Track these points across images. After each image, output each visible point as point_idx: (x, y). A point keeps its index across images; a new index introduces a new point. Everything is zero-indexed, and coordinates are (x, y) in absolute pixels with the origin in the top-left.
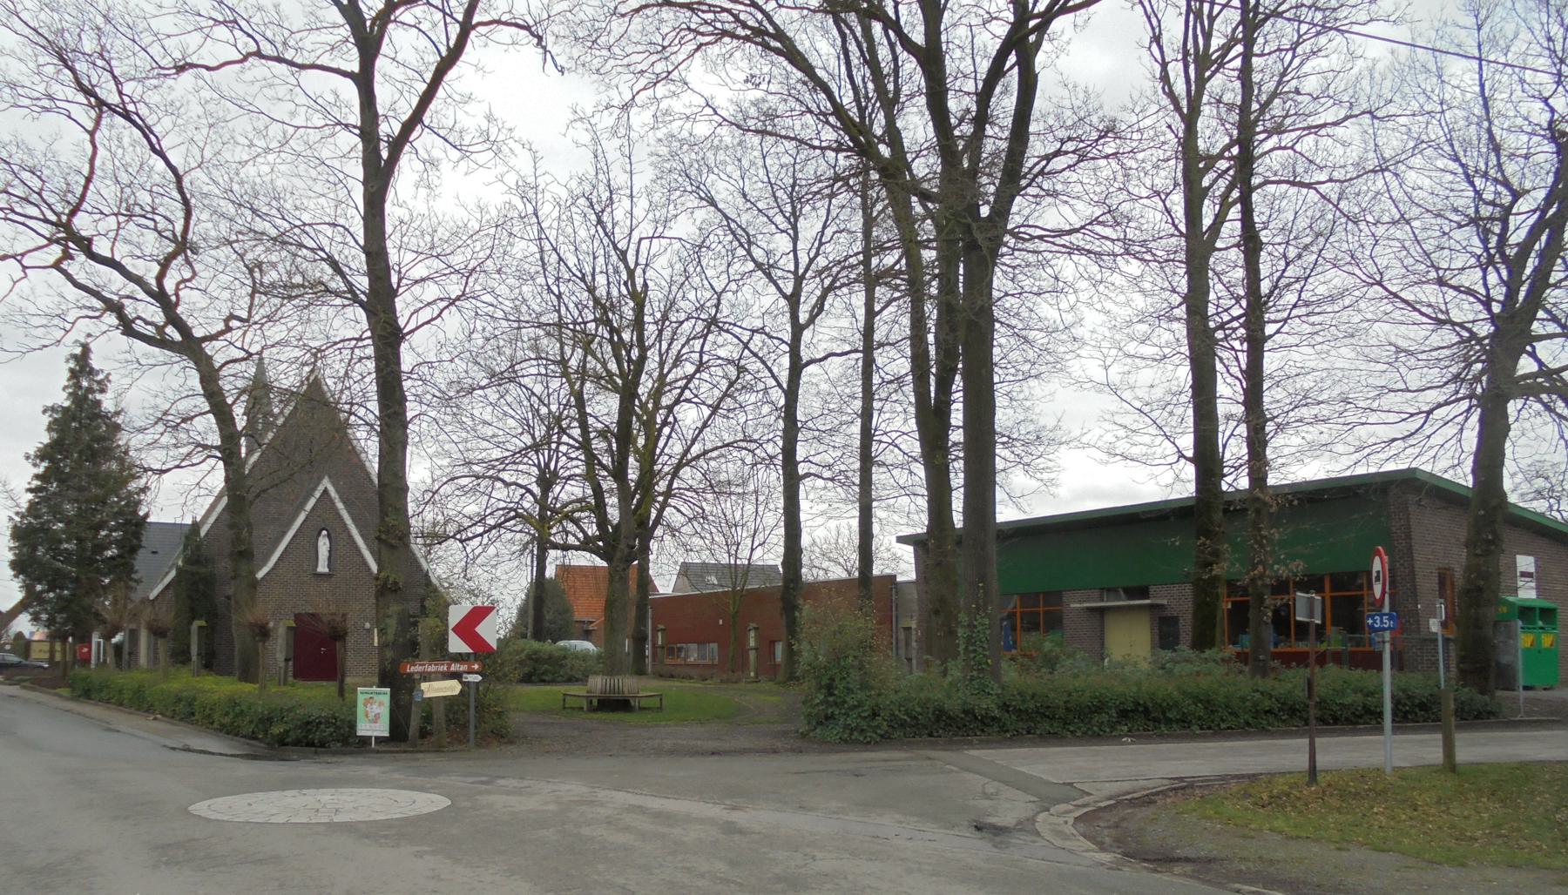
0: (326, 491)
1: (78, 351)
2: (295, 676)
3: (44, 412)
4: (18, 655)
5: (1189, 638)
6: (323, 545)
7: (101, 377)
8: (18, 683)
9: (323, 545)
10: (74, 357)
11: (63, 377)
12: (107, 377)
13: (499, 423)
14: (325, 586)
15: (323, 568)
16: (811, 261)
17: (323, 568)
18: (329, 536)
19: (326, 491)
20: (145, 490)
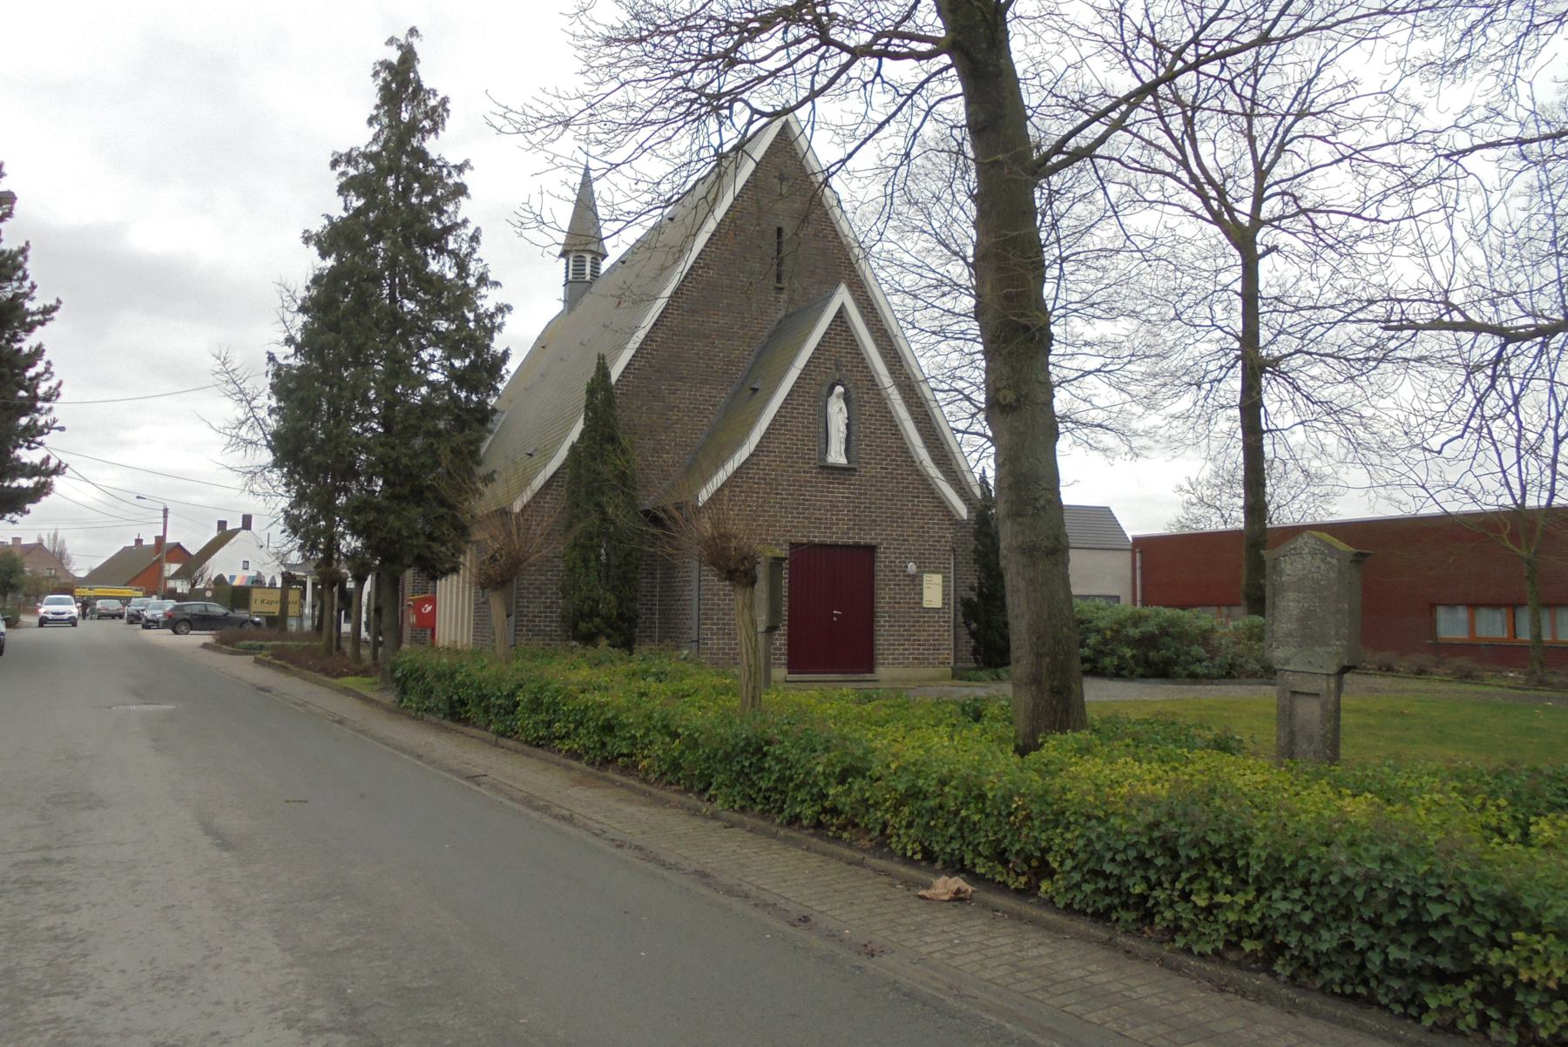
0: (841, 312)
1: (394, 56)
2: (793, 667)
3: (334, 164)
4: (224, 605)
5: (784, 659)
6: (837, 414)
7: (432, 102)
8: (248, 651)
9: (837, 414)
10: (386, 65)
11: (369, 96)
12: (444, 101)
13: (1073, 222)
14: (839, 492)
15: (837, 456)
16: (1168, 131)
17: (837, 456)
18: (847, 398)
19: (841, 312)
20: (503, 309)
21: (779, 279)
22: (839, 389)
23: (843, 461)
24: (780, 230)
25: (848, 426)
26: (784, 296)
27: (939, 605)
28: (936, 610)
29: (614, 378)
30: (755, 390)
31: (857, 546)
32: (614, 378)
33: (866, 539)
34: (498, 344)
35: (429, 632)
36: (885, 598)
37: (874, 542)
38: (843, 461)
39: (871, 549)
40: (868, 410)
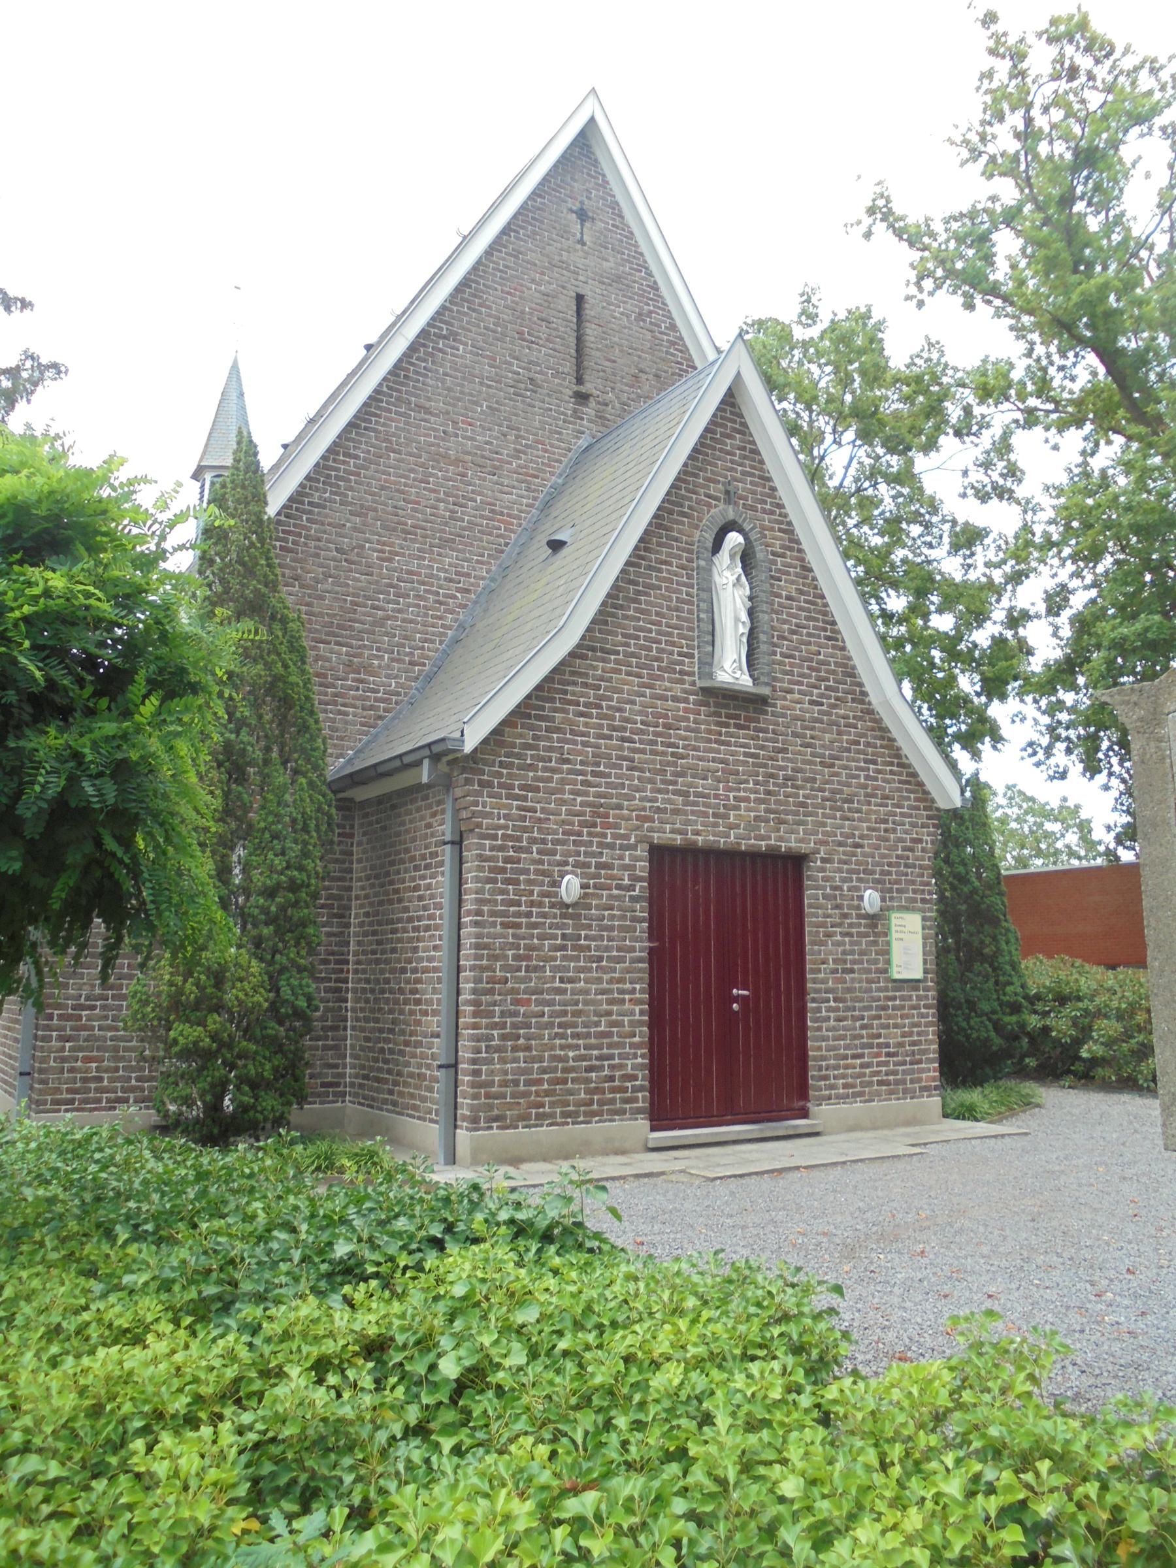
5: (642, 1099)
15: (731, 669)
18: (747, 558)
21: (580, 380)
22: (734, 539)
23: (745, 681)
24: (580, 299)
25: (751, 613)
26: (589, 411)
27: (919, 975)
28: (914, 984)
29: (272, 510)
30: (556, 546)
31: (1144, 947)
32: (272, 510)
33: (791, 843)
34: (813, 1108)
35: (361, 794)
36: (823, 957)
37: (804, 848)
38: (745, 681)
39: (796, 863)
40: (786, 588)
